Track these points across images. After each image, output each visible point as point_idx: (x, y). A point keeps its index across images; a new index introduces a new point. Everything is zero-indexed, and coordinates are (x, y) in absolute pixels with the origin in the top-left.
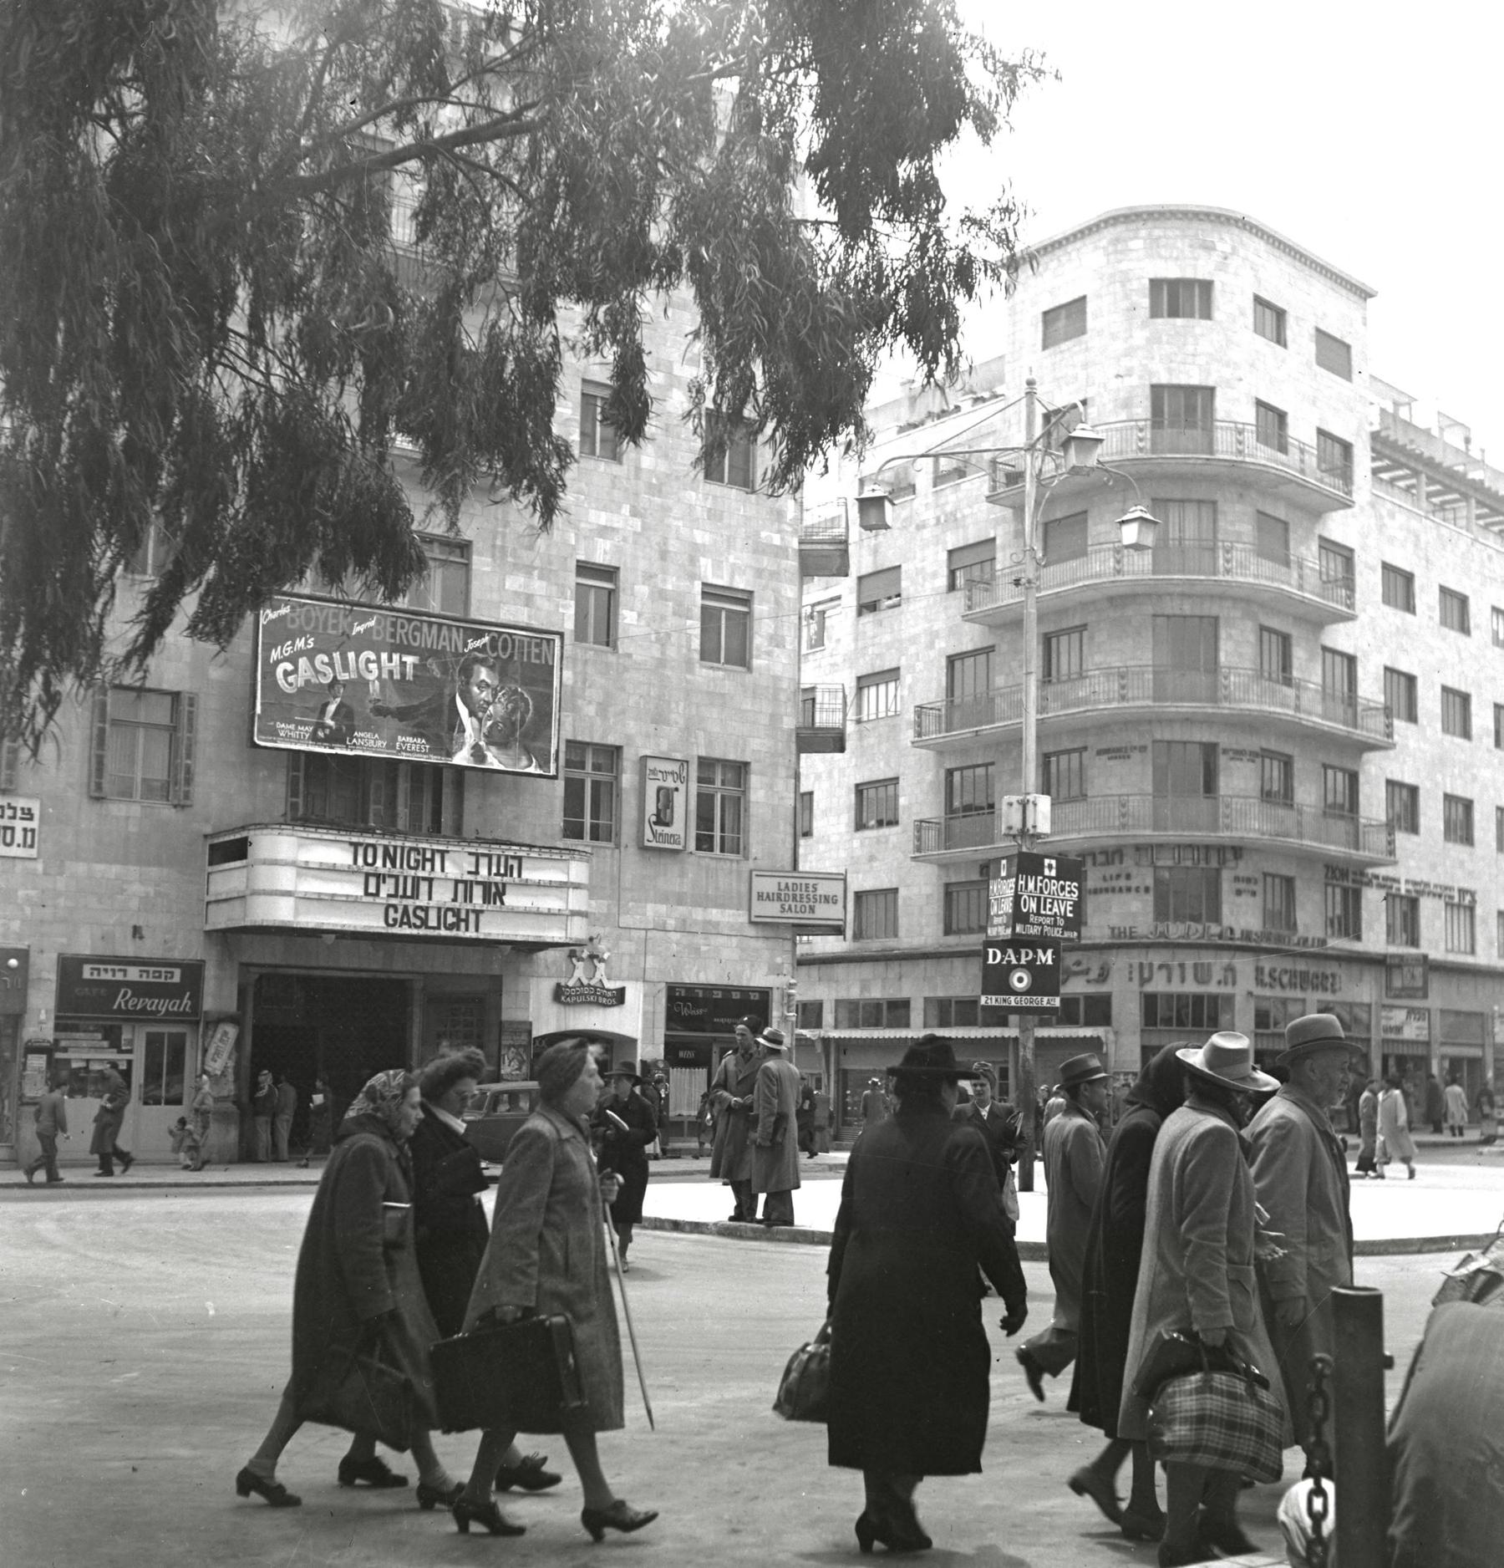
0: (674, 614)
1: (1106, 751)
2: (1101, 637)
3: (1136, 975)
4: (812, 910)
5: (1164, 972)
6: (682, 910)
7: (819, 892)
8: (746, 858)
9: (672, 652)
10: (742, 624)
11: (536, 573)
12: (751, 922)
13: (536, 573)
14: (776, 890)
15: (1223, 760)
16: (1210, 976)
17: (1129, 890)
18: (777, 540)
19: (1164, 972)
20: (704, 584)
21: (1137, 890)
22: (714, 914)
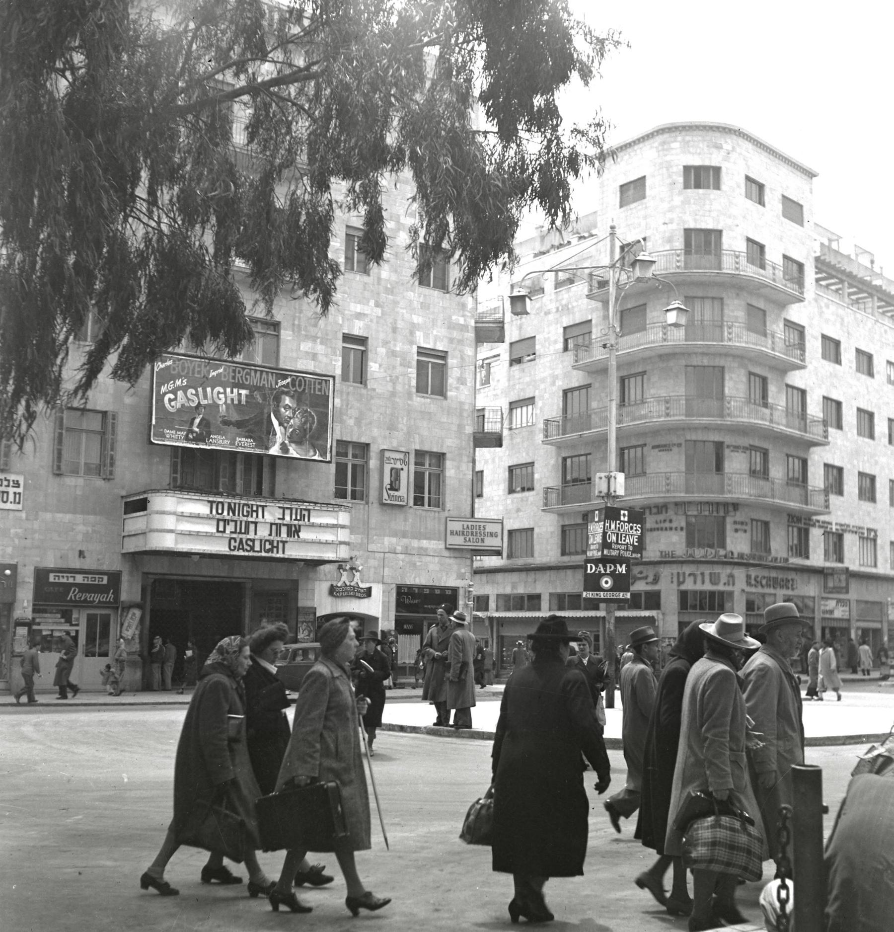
0: (401, 365)
1: (658, 447)
2: (654, 379)
3: (675, 580)
4: (483, 541)
5: (692, 578)
6: (405, 541)
7: (487, 530)
8: (444, 510)
9: (399, 388)
10: (441, 371)
11: (318, 340)
12: (446, 548)
13: (318, 340)
14: (461, 529)
15: (727, 452)
16: (719, 580)
17: (671, 529)
18: (462, 321)
19: (692, 578)
20: (419, 347)
21: (676, 529)
22: (425, 543)
